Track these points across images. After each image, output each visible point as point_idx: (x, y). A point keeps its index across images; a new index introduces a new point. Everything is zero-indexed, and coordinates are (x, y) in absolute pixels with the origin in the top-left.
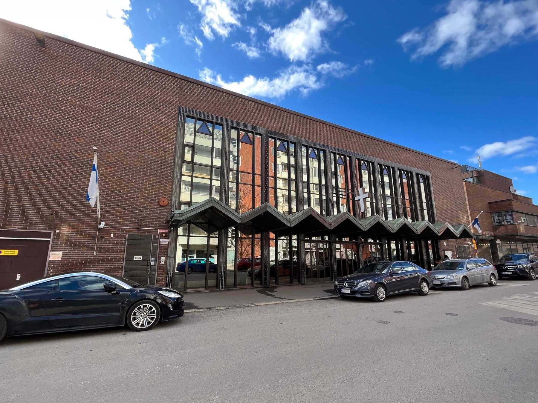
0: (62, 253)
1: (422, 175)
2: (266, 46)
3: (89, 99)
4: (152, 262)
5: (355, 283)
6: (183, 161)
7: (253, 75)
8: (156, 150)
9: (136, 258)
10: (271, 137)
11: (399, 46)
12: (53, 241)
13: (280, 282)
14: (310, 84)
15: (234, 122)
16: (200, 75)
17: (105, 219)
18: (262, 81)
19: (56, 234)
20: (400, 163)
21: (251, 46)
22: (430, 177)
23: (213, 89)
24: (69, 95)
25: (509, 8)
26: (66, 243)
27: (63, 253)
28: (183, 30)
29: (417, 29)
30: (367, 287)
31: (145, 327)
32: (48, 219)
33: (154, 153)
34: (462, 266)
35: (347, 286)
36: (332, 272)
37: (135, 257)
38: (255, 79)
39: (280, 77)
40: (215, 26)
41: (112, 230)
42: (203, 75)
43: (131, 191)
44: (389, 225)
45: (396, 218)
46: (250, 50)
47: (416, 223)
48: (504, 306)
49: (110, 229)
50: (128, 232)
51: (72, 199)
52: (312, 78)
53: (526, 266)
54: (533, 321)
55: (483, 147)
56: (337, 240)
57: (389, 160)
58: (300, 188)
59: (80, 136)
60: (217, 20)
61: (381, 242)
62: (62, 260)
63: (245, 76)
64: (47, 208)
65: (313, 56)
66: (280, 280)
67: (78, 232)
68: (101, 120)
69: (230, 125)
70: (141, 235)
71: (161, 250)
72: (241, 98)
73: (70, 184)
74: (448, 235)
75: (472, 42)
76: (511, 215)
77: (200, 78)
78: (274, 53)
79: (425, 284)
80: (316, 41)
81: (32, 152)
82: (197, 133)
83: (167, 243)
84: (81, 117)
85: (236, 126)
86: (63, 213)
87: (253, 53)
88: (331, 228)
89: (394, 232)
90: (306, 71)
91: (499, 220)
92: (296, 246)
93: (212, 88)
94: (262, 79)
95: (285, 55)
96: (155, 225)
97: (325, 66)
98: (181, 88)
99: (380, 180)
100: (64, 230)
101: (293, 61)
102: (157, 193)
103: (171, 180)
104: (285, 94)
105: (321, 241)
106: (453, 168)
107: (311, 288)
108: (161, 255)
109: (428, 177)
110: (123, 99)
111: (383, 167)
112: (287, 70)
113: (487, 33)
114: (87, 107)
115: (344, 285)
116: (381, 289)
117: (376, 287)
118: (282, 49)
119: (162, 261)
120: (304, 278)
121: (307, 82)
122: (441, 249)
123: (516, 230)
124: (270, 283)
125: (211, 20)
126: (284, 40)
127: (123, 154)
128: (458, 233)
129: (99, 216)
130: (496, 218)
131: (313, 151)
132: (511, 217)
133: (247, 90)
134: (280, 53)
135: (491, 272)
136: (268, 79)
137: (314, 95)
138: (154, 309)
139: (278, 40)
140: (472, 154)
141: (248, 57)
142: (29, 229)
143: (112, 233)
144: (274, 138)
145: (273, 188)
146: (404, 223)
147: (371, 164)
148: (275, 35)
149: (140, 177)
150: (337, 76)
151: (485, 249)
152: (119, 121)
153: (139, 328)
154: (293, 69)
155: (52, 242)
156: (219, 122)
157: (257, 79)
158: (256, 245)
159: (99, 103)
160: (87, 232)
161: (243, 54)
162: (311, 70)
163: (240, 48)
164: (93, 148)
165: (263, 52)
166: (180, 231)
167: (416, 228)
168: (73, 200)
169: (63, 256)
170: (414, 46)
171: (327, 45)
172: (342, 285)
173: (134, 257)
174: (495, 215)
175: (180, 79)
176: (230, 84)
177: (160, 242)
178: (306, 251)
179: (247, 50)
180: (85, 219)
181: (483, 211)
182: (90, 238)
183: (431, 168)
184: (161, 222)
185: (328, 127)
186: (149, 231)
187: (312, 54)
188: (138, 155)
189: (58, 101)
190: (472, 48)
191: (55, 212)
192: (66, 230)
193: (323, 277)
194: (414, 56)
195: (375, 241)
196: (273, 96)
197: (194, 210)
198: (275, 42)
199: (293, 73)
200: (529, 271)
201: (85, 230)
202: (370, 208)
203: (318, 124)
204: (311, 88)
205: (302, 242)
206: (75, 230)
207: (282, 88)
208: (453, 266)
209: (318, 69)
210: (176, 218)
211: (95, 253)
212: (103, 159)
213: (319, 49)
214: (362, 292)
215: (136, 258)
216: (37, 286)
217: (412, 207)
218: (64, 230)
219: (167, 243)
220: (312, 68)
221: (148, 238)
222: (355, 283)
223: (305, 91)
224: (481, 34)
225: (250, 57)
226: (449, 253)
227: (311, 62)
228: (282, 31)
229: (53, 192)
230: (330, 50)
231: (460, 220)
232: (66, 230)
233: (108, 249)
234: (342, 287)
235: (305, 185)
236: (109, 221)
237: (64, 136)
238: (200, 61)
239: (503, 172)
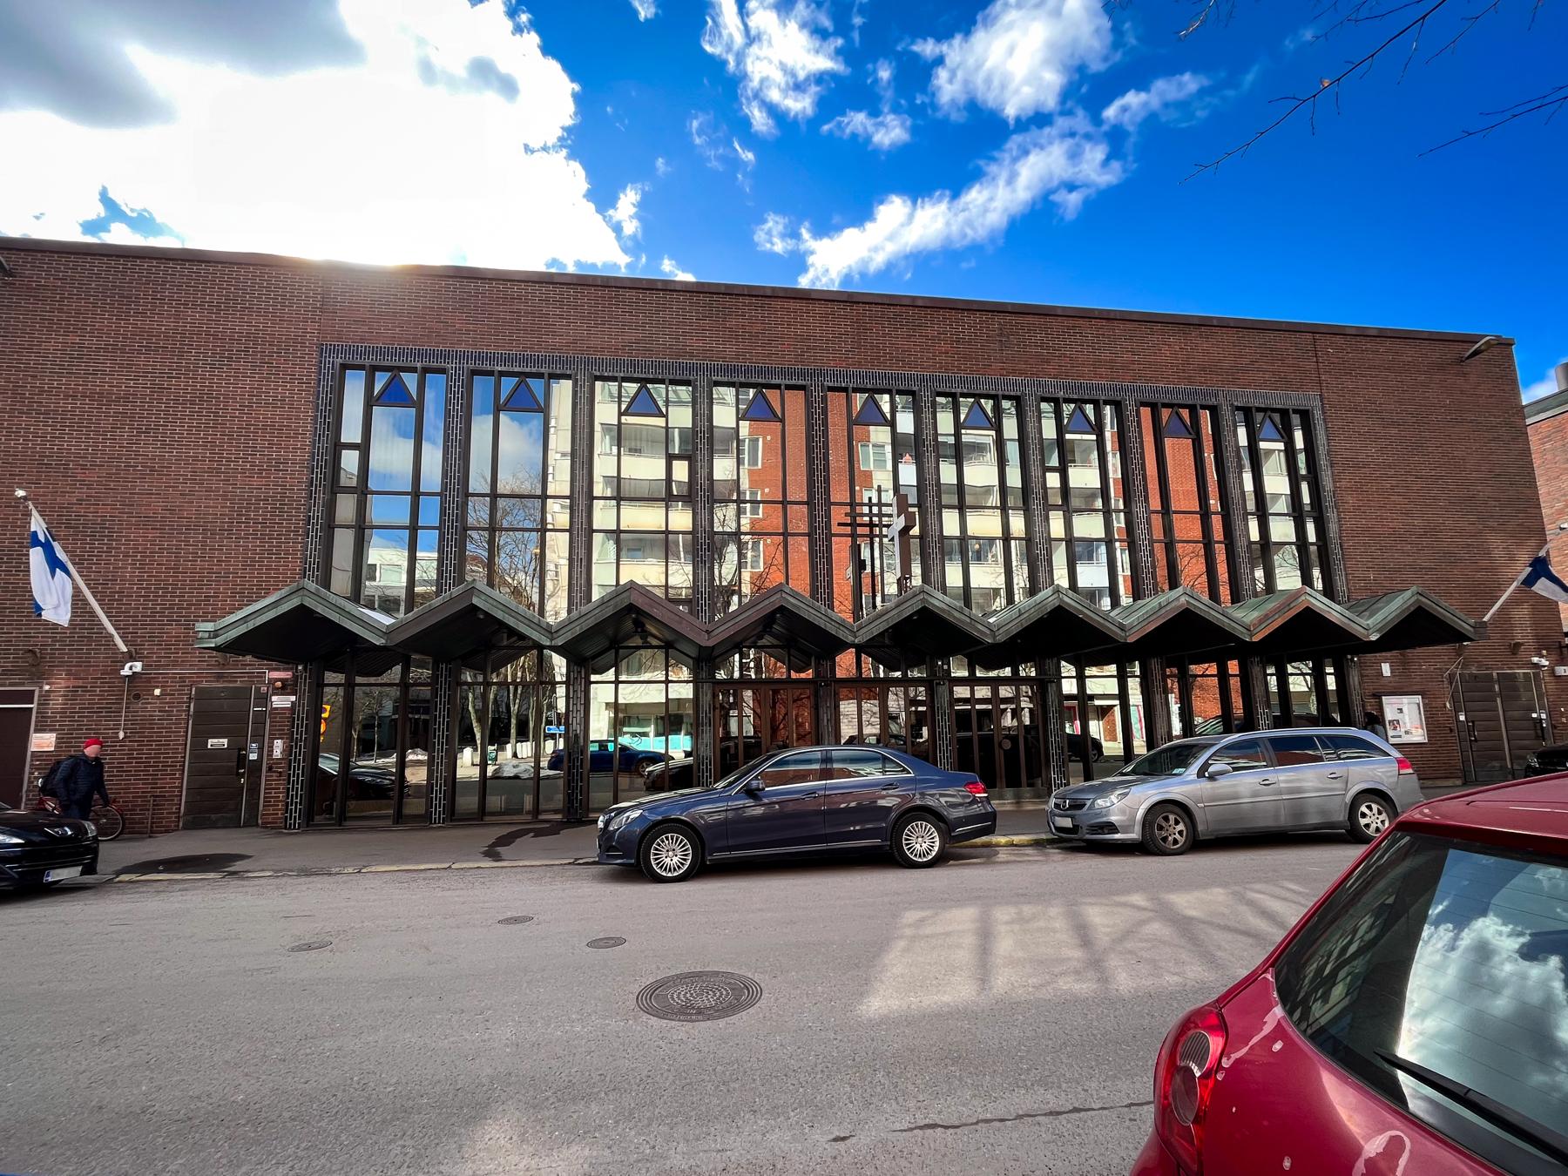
12: (38, 709)
15: (480, 357)
16: (756, 238)
17: (143, 653)
22: (1318, 414)
28: (700, 132)
32: (27, 662)
33: (256, 481)
37: (211, 741)
38: (909, 203)
39: (984, 179)
40: (774, 95)
41: (158, 678)
43: (183, 581)
46: (882, 124)
52: (1091, 150)
60: (778, 77)
68: (132, 419)
71: (273, 722)
72: (504, 280)
94: (926, 199)
97: (1133, 99)
106: (1461, 360)
110: (181, 357)
125: (762, 81)
127: (181, 495)
137: (1102, 204)
138: (904, 842)
141: (877, 151)
143: (157, 687)
148: (948, 61)
155: (37, 713)
161: (860, 144)
165: (920, 122)
173: (210, 740)
179: (871, 129)
186: (245, 677)
189: (42, 392)
191: (41, 645)
192: (63, 683)
196: (966, 242)
203: (778, 303)
204: (1086, 185)
206: (80, 683)
211: (121, 735)
221: (243, 694)
228: (966, 42)
232: (63, 683)
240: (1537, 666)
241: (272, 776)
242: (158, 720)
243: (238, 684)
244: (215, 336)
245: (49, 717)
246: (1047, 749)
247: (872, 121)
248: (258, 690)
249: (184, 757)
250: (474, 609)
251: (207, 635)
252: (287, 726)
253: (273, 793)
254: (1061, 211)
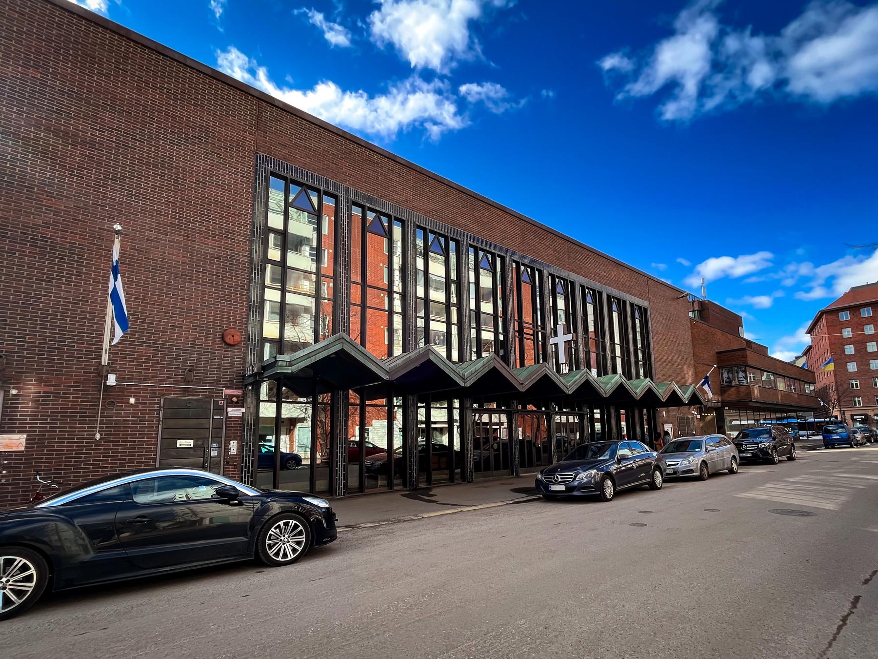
0: (25, 436)
1: (617, 298)
2: (364, 26)
3: (68, 115)
4: (213, 450)
5: (572, 475)
6: (266, 260)
7: (335, 82)
8: (214, 235)
9: (182, 443)
11: (598, 72)
14: (445, 118)
15: (356, 194)
16: (220, 61)
19: (10, 396)
21: (335, 22)
22: (649, 310)
23: (319, 126)
24: (24, 102)
25: (757, 44)
26: (34, 417)
29: (627, 49)
30: (591, 480)
31: (289, 558)
34: (700, 447)
35: (560, 480)
36: (512, 462)
38: (340, 90)
39: (388, 95)
42: (225, 63)
46: (331, 29)
47: (603, 379)
48: (764, 497)
49: (127, 389)
50: (164, 394)
52: (448, 105)
53: (769, 445)
54: (806, 512)
55: (706, 261)
56: (520, 407)
57: (595, 279)
58: (466, 319)
59: (53, 193)
63: (320, 82)
65: (454, 64)
66: (435, 476)
69: (351, 199)
74: (674, 400)
75: (704, 90)
76: (745, 372)
77: (220, 66)
78: (379, 44)
79: (658, 473)
80: (460, 36)
82: (292, 211)
83: (241, 415)
84: (52, 152)
85: (360, 201)
86: (23, 353)
87: (337, 36)
89: (608, 395)
90: (439, 92)
91: (728, 378)
94: (354, 94)
95: (400, 50)
97: (474, 88)
98: (259, 117)
99: (551, 305)
100: (29, 388)
101: (415, 66)
103: (245, 295)
104: (396, 130)
106: (678, 298)
107: (485, 487)
109: (645, 309)
111: (557, 280)
113: (726, 78)
114: (66, 134)
115: (554, 478)
117: (603, 480)
118: (396, 39)
119: (232, 449)
120: (471, 471)
121: (439, 112)
122: (659, 421)
123: (749, 393)
126: (399, 21)
127: (147, 239)
128: (685, 397)
129: (105, 360)
130: (725, 375)
131: (485, 257)
132: (744, 375)
133: (322, 111)
134: (390, 46)
136: (365, 95)
137: (449, 136)
139: (389, 19)
140: (690, 271)
141: (326, 43)
143: (131, 396)
144: (362, 207)
146: (620, 382)
148: (383, 9)
151: (710, 421)
152: (136, 171)
153: (281, 560)
154: (416, 84)
157: (344, 91)
159: (91, 128)
160: (78, 394)
161: (317, 33)
162: (447, 91)
163: (310, 21)
165: (357, 37)
169: (27, 443)
170: (620, 79)
171: (478, 48)
172: (551, 478)
173: (178, 441)
174: (724, 370)
175: (257, 98)
177: (227, 413)
178: (494, 427)
179: (324, 27)
180: (72, 368)
181: (715, 366)
182: (87, 405)
183: (650, 296)
185: (508, 218)
187: (452, 59)
188: (179, 242)
190: (705, 100)
192: (33, 389)
194: (620, 97)
195: (573, 409)
197: (311, 355)
198: (382, 21)
199: (414, 90)
200: (772, 452)
202: (401, 332)
203: (493, 210)
204: (446, 125)
205: (469, 413)
206: (52, 389)
208: (682, 447)
209: (460, 91)
210: (281, 369)
211: (98, 436)
213: (464, 52)
214: (584, 488)
215: (182, 443)
216: (87, 499)
217: (624, 356)
218: (29, 388)
219: (241, 415)
220: (449, 88)
222: (572, 475)
223: (435, 129)
224: (718, 78)
225: (331, 43)
226: (668, 428)
230: (483, 58)
232: (33, 389)
234: (552, 482)
235: (421, 304)
236: (125, 371)
237: (16, 191)
238: (221, 30)
239: (729, 304)
240: (693, 414)
243: (200, 397)
245: (18, 419)
248: (216, 403)
249: (156, 455)
251: (284, 364)
252: (239, 430)
253: (156, 489)
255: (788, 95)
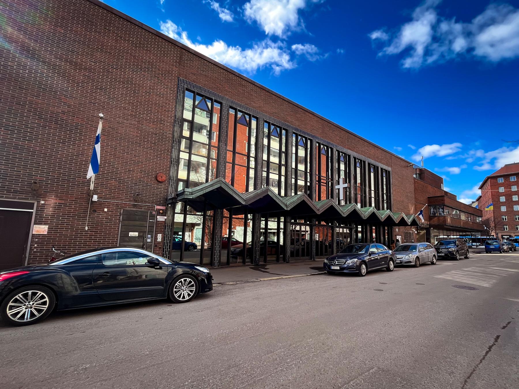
0: (47, 226)
1: (373, 165)
2: (241, 11)
5: (344, 261)
6: (182, 137)
8: (154, 122)
9: (131, 234)
10: (231, 107)
11: (369, 41)
12: (36, 212)
13: (269, 261)
14: (283, 63)
15: (232, 102)
16: (162, 28)
18: (233, 50)
20: (369, 158)
21: (225, 8)
22: (391, 172)
23: (213, 64)
24: (54, 45)
25: (458, 27)
26: (53, 216)
27: (49, 226)
31: (186, 299)
35: (337, 263)
38: (226, 46)
39: (252, 49)
41: (105, 203)
42: (165, 29)
44: (362, 212)
45: (347, 203)
46: (223, 12)
47: (364, 209)
50: (123, 207)
51: (58, 166)
52: (285, 56)
53: (454, 250)
55: (424, 147)
61: (311, 223)
62: (48, 234)
64: (28, 175)
65: (289, 33)
66: (269, 258)
67: (67, 204)
69: (229, 105)
70: (137, 210)
71: (157, 227)
73: (56, 150)
75: (427, 52)
76: (443, 209)
78: (248, 21)
79: (391, 262)
80: (293, 18)
81: (8, 108)
85: (234, 106)
87: (226, 16)
88: (319, 213)
89: (366, 218)
90: (280, 48)
92: (264, 227)
93: (212, 63)
94: (234, 48)
95: (260, 25)
96: (152, 201)
97: (300, 47)
98: (181, 58)
99: (337, 167)
101: (268, 34)
102: (154, 168)
103: (169, 155)
104: (256, 68)
105: (304, 224)
107: (296, 265)
108: (158, 232)
110: (118, 59)
111: (341, 154)
112: (261, 43)
113: (440, 46)
114: (76, 63)
115: (334, 262)
116: (364, 266)
118: (258, 18)
119: (159, 238)
122: (394, 234)
123: (445, 220)
124: (259, 262)
126: (260, 9)
127: (118, 123)
128: (409, 221)
130: (432, 210)
132: (442, 210)
133: (216, 56)
134: (255, 22)
135: (433, 254)
136: (240, 49)
137: (285, 73)
139: (254, 7)
140: (415, 152)
141: (220, 19)
142: (6, 198)
143: (105, 207)
144: (235, 109)
145: (245, 167)
146: (373, 211)
147: (330, 149)
149: (137, 149)
150: (310, 60)
153: (181, 300)
155: (36, 214)
156: (218, 100)
158: (224, 223)
163: (212, 7)
164: (100, 115)
165: (236, 17)
166: (179, 207)
167: (381, 216)
168: (60, 168)
169: (49, 230)
170: (381, 44)
171: (303, 25)
172: (332, 262)
173: (130, 233)
175: (180, 47)
176: (197, 46)
177: (157, 219)
180: (74, 191)
181: (427, 205)
182: (81, 211)
184: (159, 198)
185: (316, 119)
190: (427, 58)
193: (294, 256)
194: (380, 54)
197: (203, 189)
198: (251, 8)
199: (267, 47)
200: (456, 254)
201: (75, 203)
205: (289, 224)
207: (254, 61)
208: (406, 249)
210: (186, 196)
211: (87, 228)
212: (95, 125)
213: (295, 27)
214: (350, 269)
219: (164, 220)
220: (286, 46)
222: (344, 261)
223: (278, 69)
224: (435, 46)
226: (399, 238)
227: (286, 39)
229: (35, 157)
231: (409, 211)
233: (101, 224)
234: (332, 264)
235: (265, 163)
238: (163, 11)
239: (436, 171)
240: (413, 231)
241: (157, 249)
242: (105, 222)
244: (134, 57)
246: (311, 249)
247: (221, 9)
248: (151, 213)
249: (117, 240)
250: (268, 196)
254: (274, 71)
255: (474, 56)
